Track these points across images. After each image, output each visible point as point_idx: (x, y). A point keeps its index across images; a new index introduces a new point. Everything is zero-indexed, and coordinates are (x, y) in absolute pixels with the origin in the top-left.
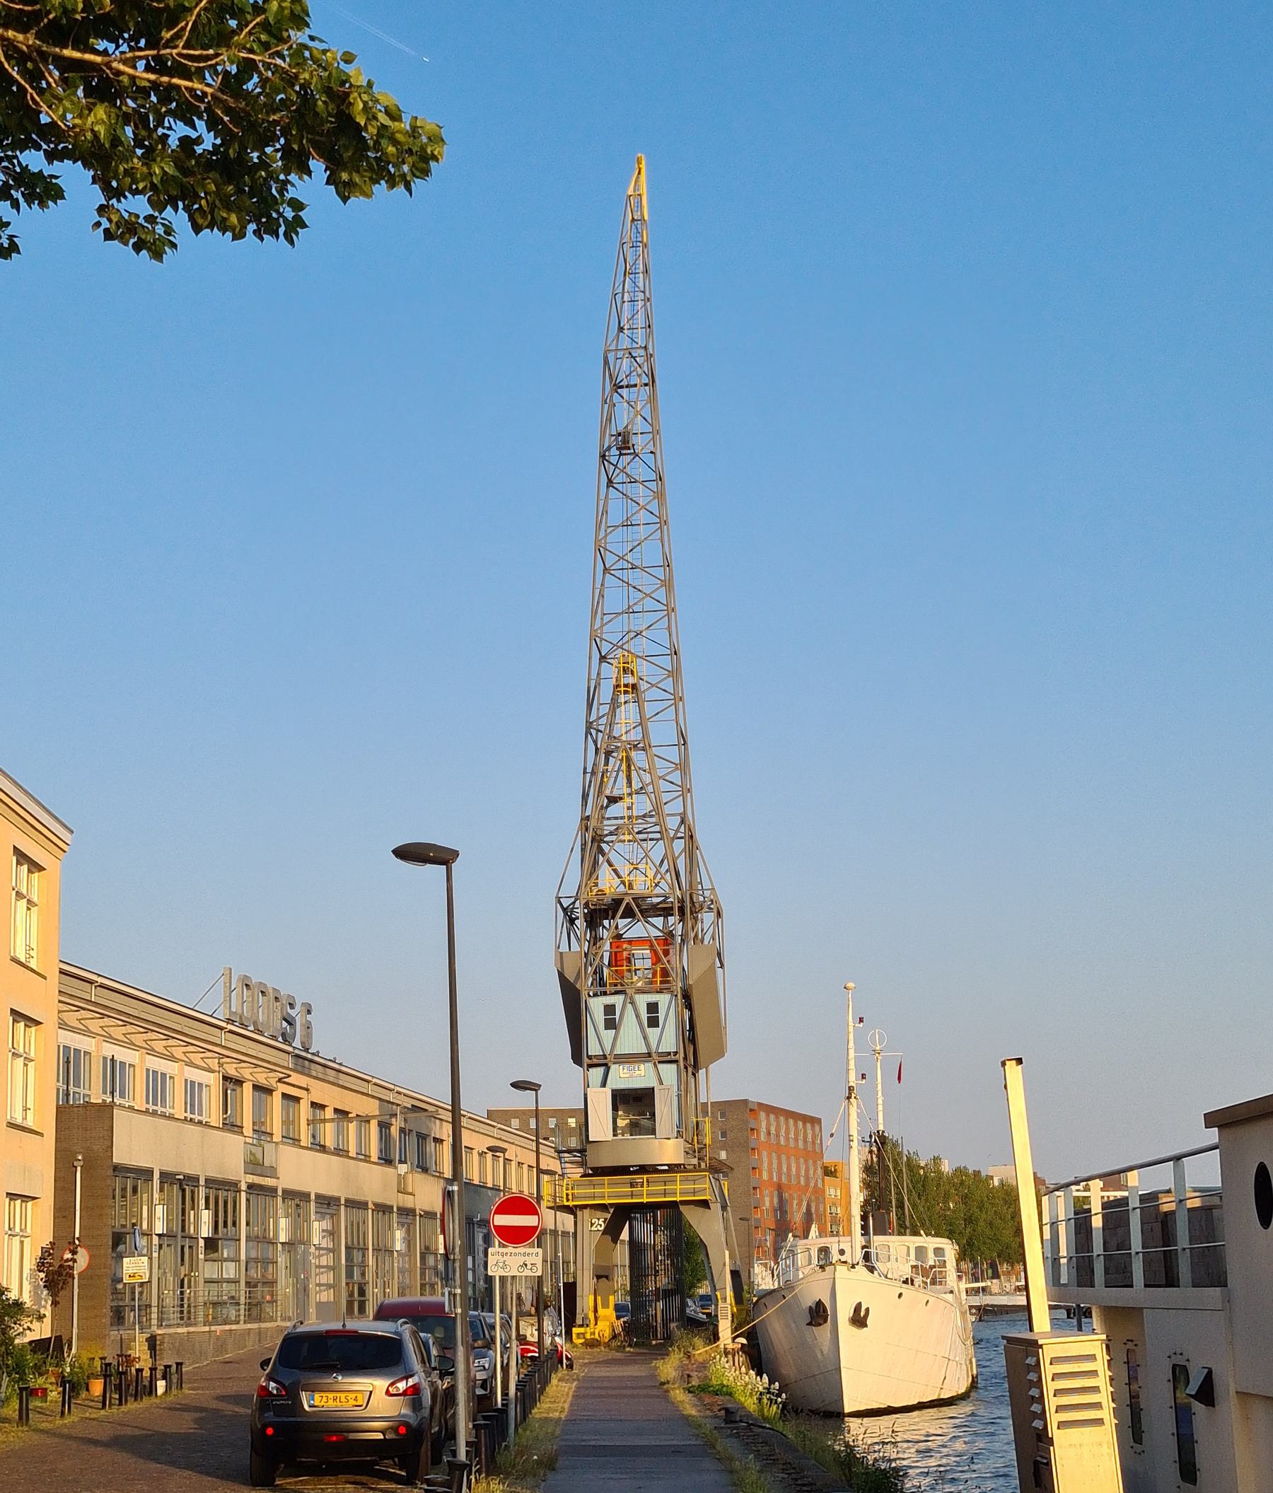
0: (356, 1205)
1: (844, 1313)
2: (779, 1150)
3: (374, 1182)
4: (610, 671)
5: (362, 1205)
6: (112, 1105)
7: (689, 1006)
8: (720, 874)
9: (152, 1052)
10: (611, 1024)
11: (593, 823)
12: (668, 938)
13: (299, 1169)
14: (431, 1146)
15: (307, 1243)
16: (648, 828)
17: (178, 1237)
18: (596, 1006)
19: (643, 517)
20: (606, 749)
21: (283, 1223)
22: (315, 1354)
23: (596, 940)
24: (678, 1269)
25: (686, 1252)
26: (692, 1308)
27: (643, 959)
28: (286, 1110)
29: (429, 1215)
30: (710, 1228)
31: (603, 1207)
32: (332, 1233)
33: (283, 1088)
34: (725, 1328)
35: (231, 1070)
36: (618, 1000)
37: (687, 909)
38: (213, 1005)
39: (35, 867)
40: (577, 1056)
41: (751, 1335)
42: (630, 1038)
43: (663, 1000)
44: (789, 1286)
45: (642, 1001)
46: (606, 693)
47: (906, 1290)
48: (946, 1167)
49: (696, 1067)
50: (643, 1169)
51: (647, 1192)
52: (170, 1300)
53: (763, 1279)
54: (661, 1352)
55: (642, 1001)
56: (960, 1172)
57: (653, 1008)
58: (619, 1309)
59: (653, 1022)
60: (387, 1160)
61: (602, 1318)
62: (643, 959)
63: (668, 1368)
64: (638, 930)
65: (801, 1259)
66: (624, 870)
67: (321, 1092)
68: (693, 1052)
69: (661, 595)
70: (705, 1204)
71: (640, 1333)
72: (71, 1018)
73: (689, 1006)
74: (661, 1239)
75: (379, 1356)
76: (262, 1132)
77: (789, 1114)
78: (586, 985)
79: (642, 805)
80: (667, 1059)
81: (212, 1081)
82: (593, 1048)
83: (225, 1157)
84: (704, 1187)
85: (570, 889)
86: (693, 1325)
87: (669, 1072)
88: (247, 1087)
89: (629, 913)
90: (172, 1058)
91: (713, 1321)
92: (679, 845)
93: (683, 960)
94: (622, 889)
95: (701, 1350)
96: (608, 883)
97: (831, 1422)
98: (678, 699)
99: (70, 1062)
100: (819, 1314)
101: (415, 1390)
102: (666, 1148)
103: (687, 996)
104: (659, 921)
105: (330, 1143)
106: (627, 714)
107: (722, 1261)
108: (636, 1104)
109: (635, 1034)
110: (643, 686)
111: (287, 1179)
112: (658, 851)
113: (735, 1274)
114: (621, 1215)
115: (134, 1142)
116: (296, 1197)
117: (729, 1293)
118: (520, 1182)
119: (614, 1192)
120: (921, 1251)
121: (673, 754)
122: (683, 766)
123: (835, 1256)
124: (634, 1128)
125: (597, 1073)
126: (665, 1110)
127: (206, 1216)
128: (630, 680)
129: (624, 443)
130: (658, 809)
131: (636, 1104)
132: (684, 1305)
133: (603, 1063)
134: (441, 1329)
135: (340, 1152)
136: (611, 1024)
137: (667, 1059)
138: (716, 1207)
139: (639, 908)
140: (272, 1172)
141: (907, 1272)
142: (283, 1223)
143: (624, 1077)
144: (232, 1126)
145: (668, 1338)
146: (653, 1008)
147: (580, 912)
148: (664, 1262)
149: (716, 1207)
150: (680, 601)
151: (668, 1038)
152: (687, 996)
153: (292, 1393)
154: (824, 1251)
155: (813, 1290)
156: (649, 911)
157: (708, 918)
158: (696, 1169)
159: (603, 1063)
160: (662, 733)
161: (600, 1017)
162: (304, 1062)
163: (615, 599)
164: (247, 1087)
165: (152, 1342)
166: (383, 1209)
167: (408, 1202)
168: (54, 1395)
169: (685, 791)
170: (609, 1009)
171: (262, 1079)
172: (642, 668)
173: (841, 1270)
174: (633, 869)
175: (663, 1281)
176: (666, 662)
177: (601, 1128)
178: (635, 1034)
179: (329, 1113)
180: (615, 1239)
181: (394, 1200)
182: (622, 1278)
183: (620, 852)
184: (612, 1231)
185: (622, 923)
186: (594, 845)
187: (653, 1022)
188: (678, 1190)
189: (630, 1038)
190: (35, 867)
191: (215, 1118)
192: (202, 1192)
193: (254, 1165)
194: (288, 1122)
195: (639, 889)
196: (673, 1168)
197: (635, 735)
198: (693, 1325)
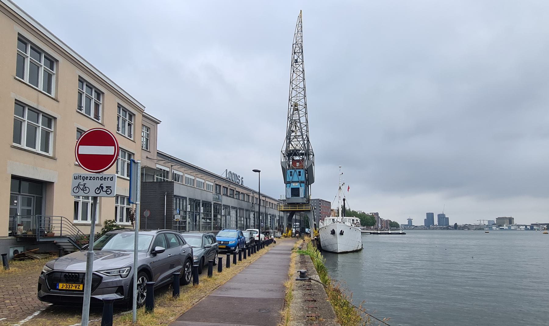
5: (243, 209)
6: (173, 182)
10: (291, 175)
12: (303, 159)
18: (289, 172)
20: (293, 122)
23: (289, 159)
36: (293, 171)
38: (224, 176)
42: (296, 178)
43: (302, 171)
45: (298, 171)
48: (351, 210)
55: (298, 171)
56: (353, 211)
57: (300, 172)
59: (300, 175)
97: (334, 255)
98: (306, 113)
116: (226, 207)
120: (353, 220)
123: (335, 221)
125: (288, 185)
129: (296, 61)
134: (19, 233)
136: (291, 175)
143: (295, 185)
146: (300, 172)
154: (333, 220)
160: (303, 120)
163: (294, 93)
170: (291, 172)
174: (297, 144)
186: (289, 139)
187: (300, 175)
192: (223, 207)
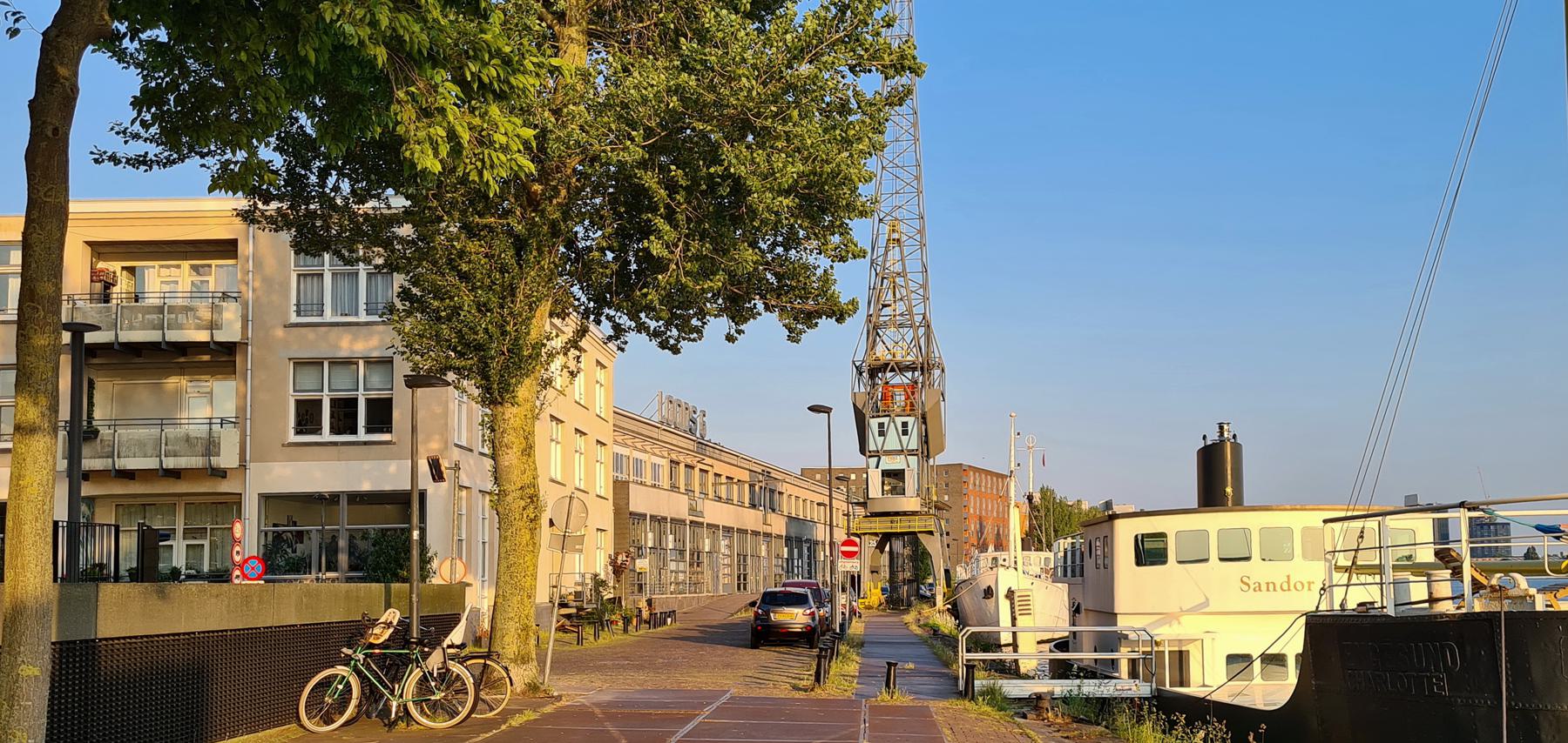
0: (742, 531)
1: (1002, 592)
2: (980, 495)
3: (751, 519)
4: (886, 229)
7: (925, 422)
8: (943, 349)
9: (636, 448)
10: (882, 433)
11: (874, 319)
13: (715, 513)
14: (776, 496)
15: (718, 552)
16: (905, 321)
17: (659, 548)
19: (905, 137)
21: (650, 535)
22: (773, 600)
23: (874, 385)
24: (915, 568)
25: (920, 558)
26: (924, 590)
27: (900, 399)
28: (701, 478)
29: (780, 537)
30: (933, 546)
31: (876, 534)
32: (729, 547)
33: (700, 466)
34: (939, 599)
35: (674, 457)
37: (925, 368)
38: (653, 413)
39: (603, 367)
40: (863, 450)
41: (954, 605)
42: (892, 442)
43: (910, 420)
44: (974, 578)
45: (899, 420)
46: (882, 242)
47: (1037, 581)
49: (928, 457)
50: (897, 514)
51: (900, 526)
52: (655, 580)
53: (961, 573)
54: (907, 611)
55: (899, 420)
57: (905, 424)
58: (883, 590)
59: (905, 433)
60: (753, 506)
61: (874, 593)
62: (900, 399)
63: (909, 618)
64: (897, 380)
65: (982, 564)
66: (890, 344)
67: (719, 467)
68: (927, 448)
69: (915, 183)
70: (931, 533)
71: (895, 602)
72: (619, 439)
73: (925, 422)
74: (907, 551)
75: (799, 600)
76: (689, 491)
77: (988, 472)
78: (867, 412)
79: (901, 307)
80: (912, 453)
81: (664, 463)
82: (872, 447)
83: (676, 506)
84: (931, 524)
85: (860, 357)
86: (923, 598)
87: (913, 460)
88: (682, 466)
89: (892, 370)
90: (645, 451)
91: (933, 596)
92: (921, 331)
93: (925, 398)
94: (889, 357)
95: (926, 610)
96: (880, 352)
98: (919, 192)
99: (618, 459)
100: (989, 593)
101: (813, 614)
102: (910, 503)
103: (924, 417)
104: (909, 374)
105: (724, 496)
106: (894, 254)
107: (939, 566)
108: (895, 477)
109: (894, 438)
110: (904, 238)
111: (708, 519)
112: (910, 334)
113: (947, 571)
114: (886, 538)
115: (640, 501)
116: (659, 520)
117: (943, 582)
118: (790, 508)
119: (881, 526)
121: (919, 278)
122: (924, 286)
123: (1001, 562)
124: (894, 491)
126: (910, 483)
127: (671, 538)
128: (896, 236)
130: (911, 313)
131: (895, 477)
132: (919, 589)
133: (877, 455)
135: (729, 501)
136: (882, 433)
137: (912, 453)
138: (937, 535)
139: (901, 368)
140: (701, 514)
141: (1038, 571)
142: (650, 535)
143: (889, 463)
144: (674, 488)
145: (910, 605)
146: (905, 424)
147: (865, 368)
148: (908, 565)
149: (937, 535)
150: (928, 240)
151: (913, 442)
152: (924, 417)
153: (767, 613)
154: (995, 559)
155: (986, 581)
156: (901, 368)
157: (937, 372)
158: (927, 514)
159: (877, 455)
160: (913, 265)
161: (876, 430)
162: (702, 445)
164: (682, 466)
165: (649, 602)
166: (756, 533)
167: (768, 529)
168: (621, 623)
169: (925, 299)
170: (881, 425)
171: (689, 461)
172: (902, 227)
173: (1001, 570)
175: (908, 575)
176: (914, 170)
177: (875, 491)
178: (894, 438)
179: (723, 480)
180: (882, 551)
181: (762, 528)
182: (885, 573)
183: (889, 334)
184: (880, 547)
185: (889, 375)
187: (905, 433)
188: (916, 525)
189: (892, 442)
190: (603, 367)
191: (666, 483)
193: (692, 511)
194: (703, 485)
195: (899, 358)
196: (914, 513)
197: (898, 268)
198: (923, 598)
